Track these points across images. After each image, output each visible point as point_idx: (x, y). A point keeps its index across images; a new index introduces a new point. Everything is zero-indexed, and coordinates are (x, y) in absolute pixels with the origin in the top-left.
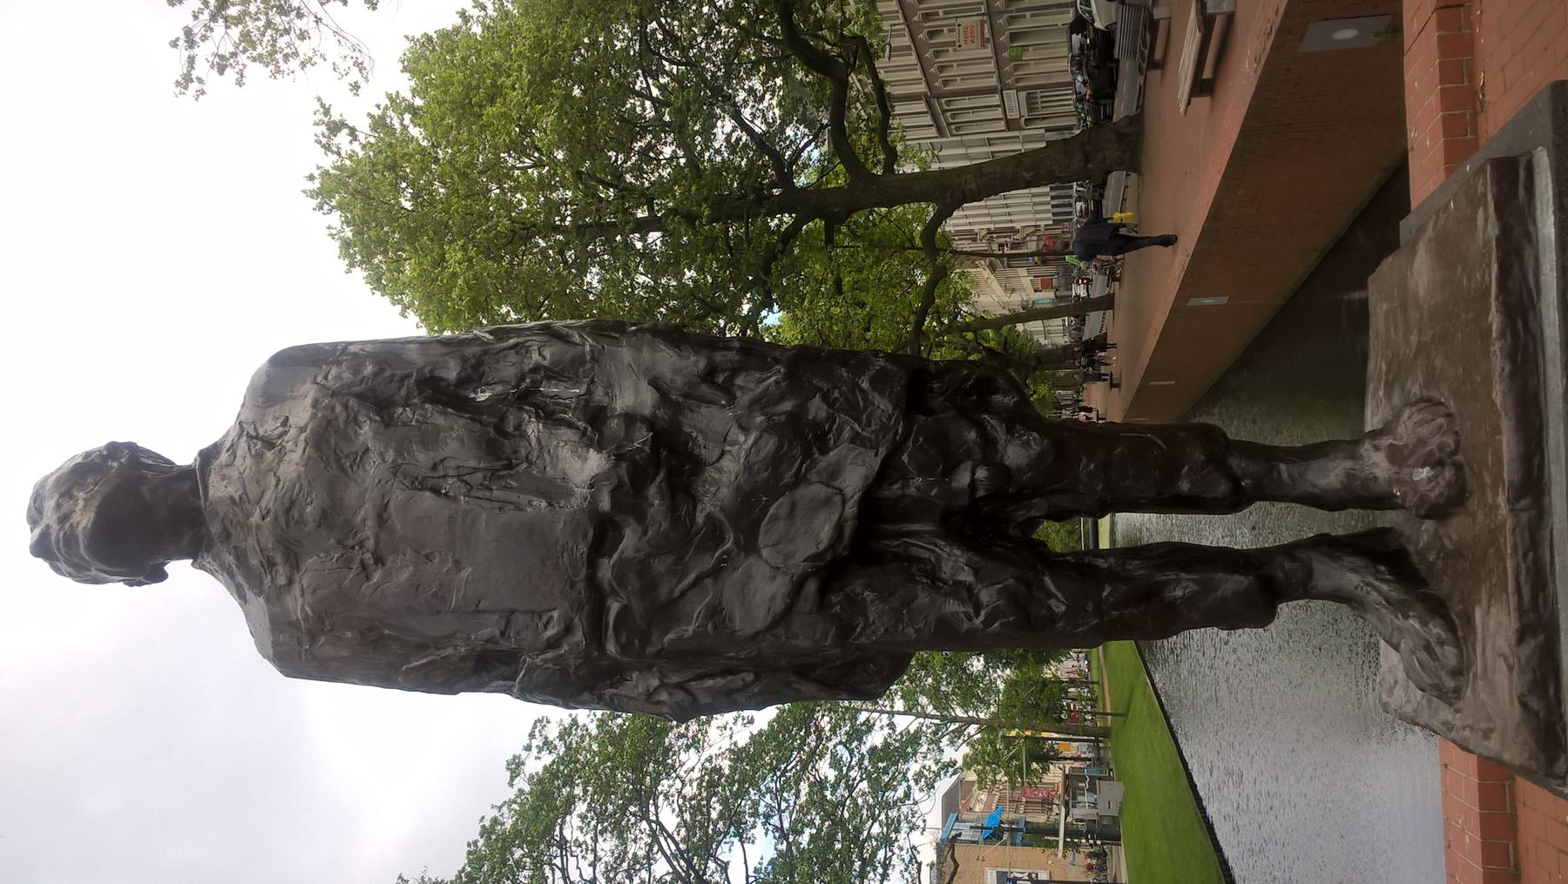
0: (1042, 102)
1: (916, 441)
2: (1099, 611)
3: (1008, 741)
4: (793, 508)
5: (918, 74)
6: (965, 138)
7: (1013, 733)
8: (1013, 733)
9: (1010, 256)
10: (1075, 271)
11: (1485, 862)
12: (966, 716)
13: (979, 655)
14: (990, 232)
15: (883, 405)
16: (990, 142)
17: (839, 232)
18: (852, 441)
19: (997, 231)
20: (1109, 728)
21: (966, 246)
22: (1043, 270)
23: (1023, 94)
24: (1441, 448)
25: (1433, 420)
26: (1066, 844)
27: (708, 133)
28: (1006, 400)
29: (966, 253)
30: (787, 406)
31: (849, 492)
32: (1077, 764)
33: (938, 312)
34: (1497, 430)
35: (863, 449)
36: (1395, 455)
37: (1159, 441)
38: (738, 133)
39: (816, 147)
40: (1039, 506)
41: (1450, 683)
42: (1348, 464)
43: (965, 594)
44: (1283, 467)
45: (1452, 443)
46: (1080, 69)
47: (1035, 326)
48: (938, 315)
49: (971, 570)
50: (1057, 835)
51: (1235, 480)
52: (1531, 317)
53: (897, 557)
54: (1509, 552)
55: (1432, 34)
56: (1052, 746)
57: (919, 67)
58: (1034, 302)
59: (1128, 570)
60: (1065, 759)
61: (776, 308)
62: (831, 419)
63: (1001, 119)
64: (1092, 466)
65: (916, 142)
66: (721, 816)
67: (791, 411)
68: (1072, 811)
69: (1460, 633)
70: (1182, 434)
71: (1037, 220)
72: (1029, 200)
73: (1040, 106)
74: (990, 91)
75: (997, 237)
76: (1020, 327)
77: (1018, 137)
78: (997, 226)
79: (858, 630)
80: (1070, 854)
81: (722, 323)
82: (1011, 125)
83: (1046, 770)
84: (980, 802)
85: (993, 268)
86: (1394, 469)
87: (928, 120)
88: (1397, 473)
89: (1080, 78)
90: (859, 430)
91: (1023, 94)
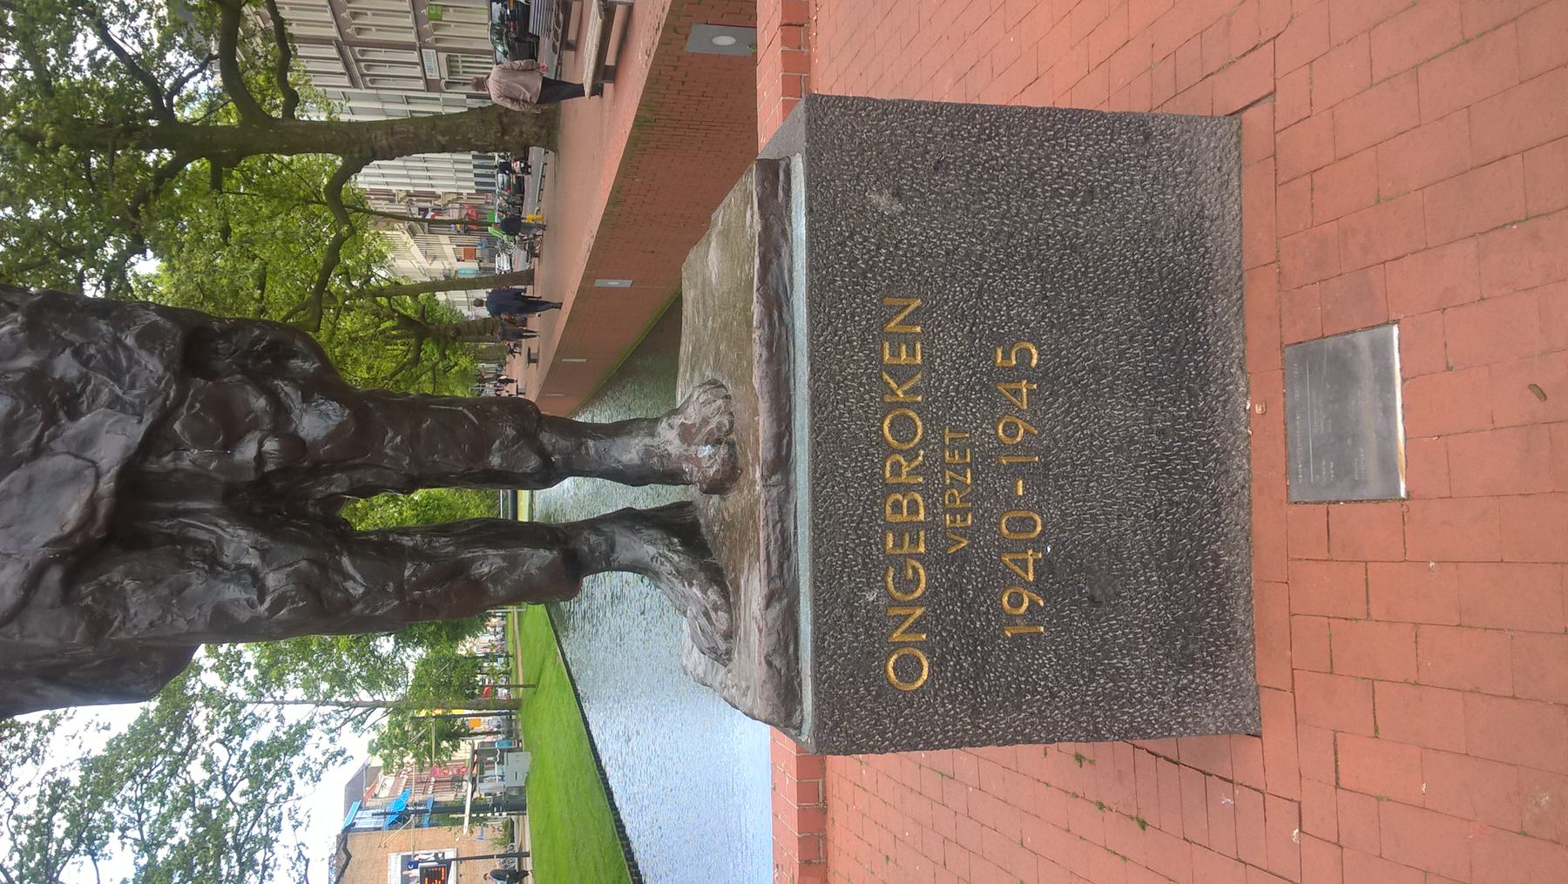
0: (464, 67)
1: (192, 406)
2: (400, 592)
3: (418, 723)
4: (30, 483)
5: (328, 16)
6: (380, 92)
7: (423, 713)
8: (423, 713)
9: (432, 222)
10: (498, 243)
11: (800, 800)
12: (371, 700)
13: (389, 635)
14: (409, 194)
15: (152, 365)
16: (408, 100)
17: (231, 177)
18: (110, 406)
19: (417, 194)
20: (520, 700)
21: (383, 206)
22: (466, 239)
23: (443, 56)
24: (719, 428)
25: (714, 401)
26: (472, 820)
27: (64, 44)
28: (306, 366)
29: (384, 215)
30: (27, 361)
31: (104, 464)
32: (489, 739)
33: (347, 273)
34: (756, 413)
35: (123, 415)
36: (686, 434)
37: (470, 415)
38: (103, 52)
39: (204, 78)
40: (339, 482)
41: (723, 646)
42: (648, 441)
43: (248, 578)
44: (591, 443)
45: (726, 422)
46: (500, 39)
47: (458, 296)
48: (347, 275)
49: (257, 553)
50: (463, 812)
51: (544, 455)
52: (785, 309)
53: (171, 539)
54: (762, 523)
55: (778, 48)
56: (463, 723)
57: (329, 9)
58: (456, 272)
59: (435, 547)
60: (476, 734)
61: (150, 253)
62: (84, 378)
63: (420, 78)
64: (399, 439)
65: (340, 90)
66: (68, 833)
67: (31, 368)
68: (479, 786)
69: (732, 600)
70: (495, 409)
71: (460, 187)
72: (450, 166)
73: (461, 70)
74: (408, 47)
75: (417, 201)
76: (441, 296)
77: (438, 99)
78: (417, 189)
79: (116, 624)
80: (477, 829)
81: (79, 266)
82: (430, 85)
83: (456, 747)
84: (387, 788)
85: (412, 233)
86: (685, 446)
87: (339, 67)
88: (686, 450)
89: (500, 48)
90: (120, 392)
91: (443, 56)
